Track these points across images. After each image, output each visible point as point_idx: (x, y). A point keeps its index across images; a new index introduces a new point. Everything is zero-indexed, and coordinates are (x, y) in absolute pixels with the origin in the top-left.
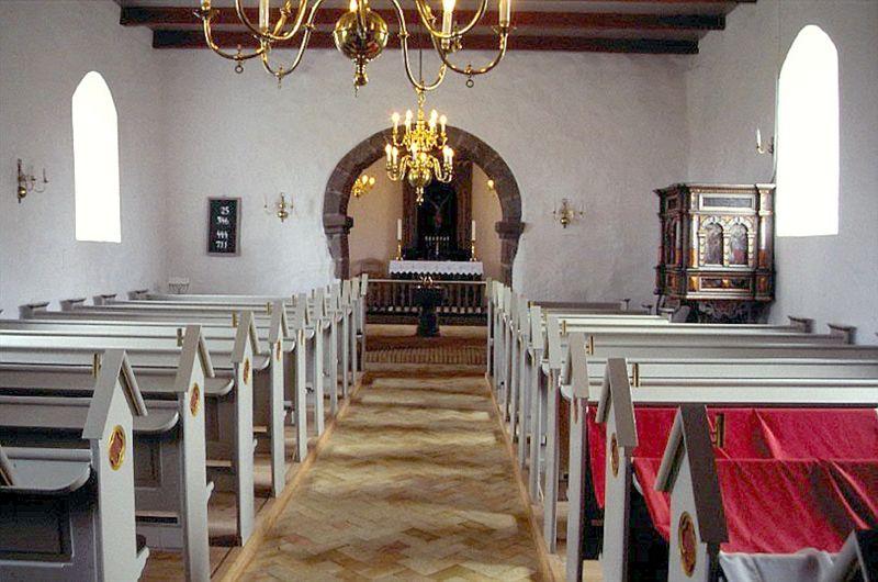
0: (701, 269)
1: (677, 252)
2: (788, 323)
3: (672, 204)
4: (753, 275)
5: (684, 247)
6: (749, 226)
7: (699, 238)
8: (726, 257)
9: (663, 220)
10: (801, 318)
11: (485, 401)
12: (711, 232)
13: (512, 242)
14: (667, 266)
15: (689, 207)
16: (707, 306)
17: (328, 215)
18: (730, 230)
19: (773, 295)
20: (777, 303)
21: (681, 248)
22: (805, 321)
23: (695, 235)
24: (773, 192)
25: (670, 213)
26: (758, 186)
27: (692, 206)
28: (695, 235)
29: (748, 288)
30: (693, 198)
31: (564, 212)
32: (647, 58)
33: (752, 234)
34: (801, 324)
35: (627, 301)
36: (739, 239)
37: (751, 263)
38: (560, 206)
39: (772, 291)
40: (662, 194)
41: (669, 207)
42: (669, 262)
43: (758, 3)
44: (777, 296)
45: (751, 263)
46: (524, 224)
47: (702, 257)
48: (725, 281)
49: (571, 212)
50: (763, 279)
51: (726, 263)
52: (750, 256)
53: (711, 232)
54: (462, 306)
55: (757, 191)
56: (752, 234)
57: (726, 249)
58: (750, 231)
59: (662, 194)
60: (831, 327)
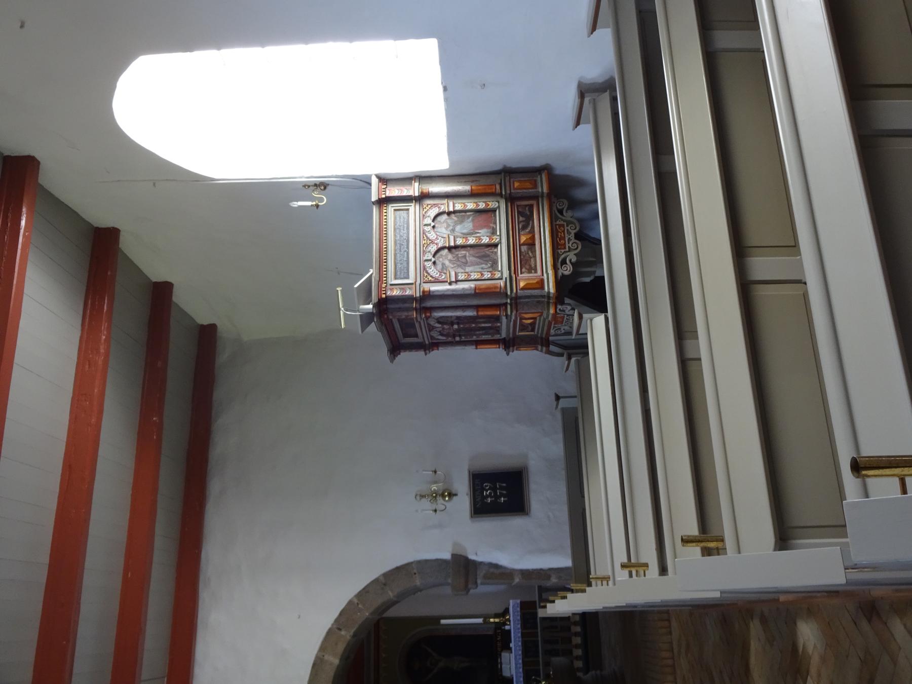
0: (506, 274)
1: (481, 313)
2: (587, 129)
3: (408, 327)
4: (511, 199)
5: (475, 302)
6: (433, 212)
7: (457, 281)
8: (485, 240)
9: (435, 345)
10: (577, 101)
11: (764, 621)
12: (447, 263)
13: (481, 573)
14: (504, 335)
15: (411, 299)
16: (564, 262)
17: (499, 324)
18: (443, 234)
19: (538, 171)
20: (549, 162)
21: (477, 307)
22: (582, 95)
23: (454, 287)
24: (384, 180)
25: (423, 336)
26: (374, 198)
27: (408, 292)
28: (454, 287)
29: (531, 206)
30: (396, 292)
31: (434, 496)
32: (219, 394)
33: (449, 206)
34: (587, 100)
35: (558, 398)
36: (456, 224)
37: (492, 204)
38: (426, 504)
39: (530, 173)
40: (395, 349)
41: (416, 336)
42: (498, 330)
43: (19, 146)
44: (538, 163)
45: (492, 204)
46: (453, 555)
47: (487, 275)
48: (523, 239)
49: (434, 487)
50: (516, 184)
51: (496, 239)
52: (482, 206)
53: (447, 263)
54: (569, 629)
55: (384, 202)
56: (449, 206)
57: (472, 241)
58: (443, 208)
59: (395, 349)
60: (578, 123)
